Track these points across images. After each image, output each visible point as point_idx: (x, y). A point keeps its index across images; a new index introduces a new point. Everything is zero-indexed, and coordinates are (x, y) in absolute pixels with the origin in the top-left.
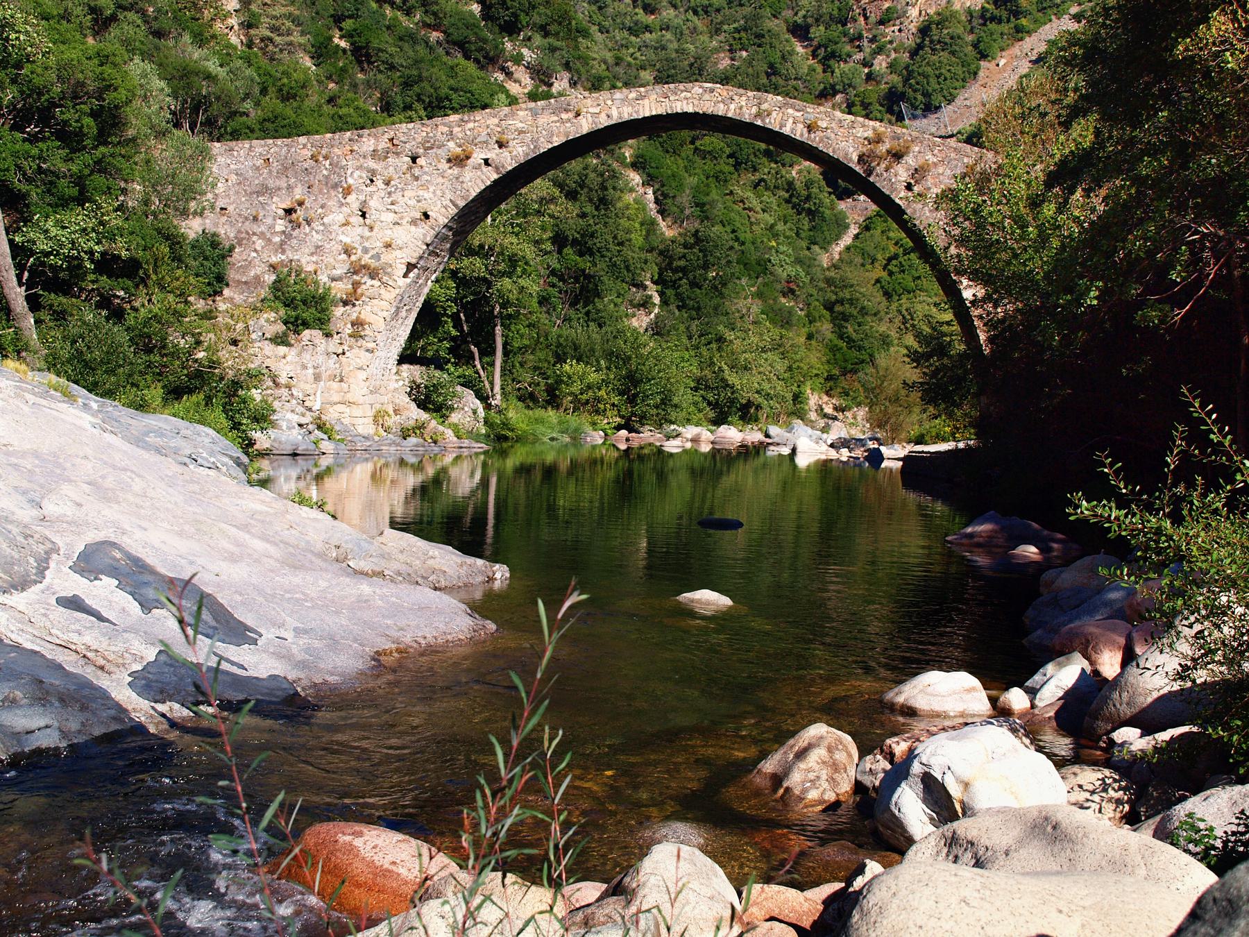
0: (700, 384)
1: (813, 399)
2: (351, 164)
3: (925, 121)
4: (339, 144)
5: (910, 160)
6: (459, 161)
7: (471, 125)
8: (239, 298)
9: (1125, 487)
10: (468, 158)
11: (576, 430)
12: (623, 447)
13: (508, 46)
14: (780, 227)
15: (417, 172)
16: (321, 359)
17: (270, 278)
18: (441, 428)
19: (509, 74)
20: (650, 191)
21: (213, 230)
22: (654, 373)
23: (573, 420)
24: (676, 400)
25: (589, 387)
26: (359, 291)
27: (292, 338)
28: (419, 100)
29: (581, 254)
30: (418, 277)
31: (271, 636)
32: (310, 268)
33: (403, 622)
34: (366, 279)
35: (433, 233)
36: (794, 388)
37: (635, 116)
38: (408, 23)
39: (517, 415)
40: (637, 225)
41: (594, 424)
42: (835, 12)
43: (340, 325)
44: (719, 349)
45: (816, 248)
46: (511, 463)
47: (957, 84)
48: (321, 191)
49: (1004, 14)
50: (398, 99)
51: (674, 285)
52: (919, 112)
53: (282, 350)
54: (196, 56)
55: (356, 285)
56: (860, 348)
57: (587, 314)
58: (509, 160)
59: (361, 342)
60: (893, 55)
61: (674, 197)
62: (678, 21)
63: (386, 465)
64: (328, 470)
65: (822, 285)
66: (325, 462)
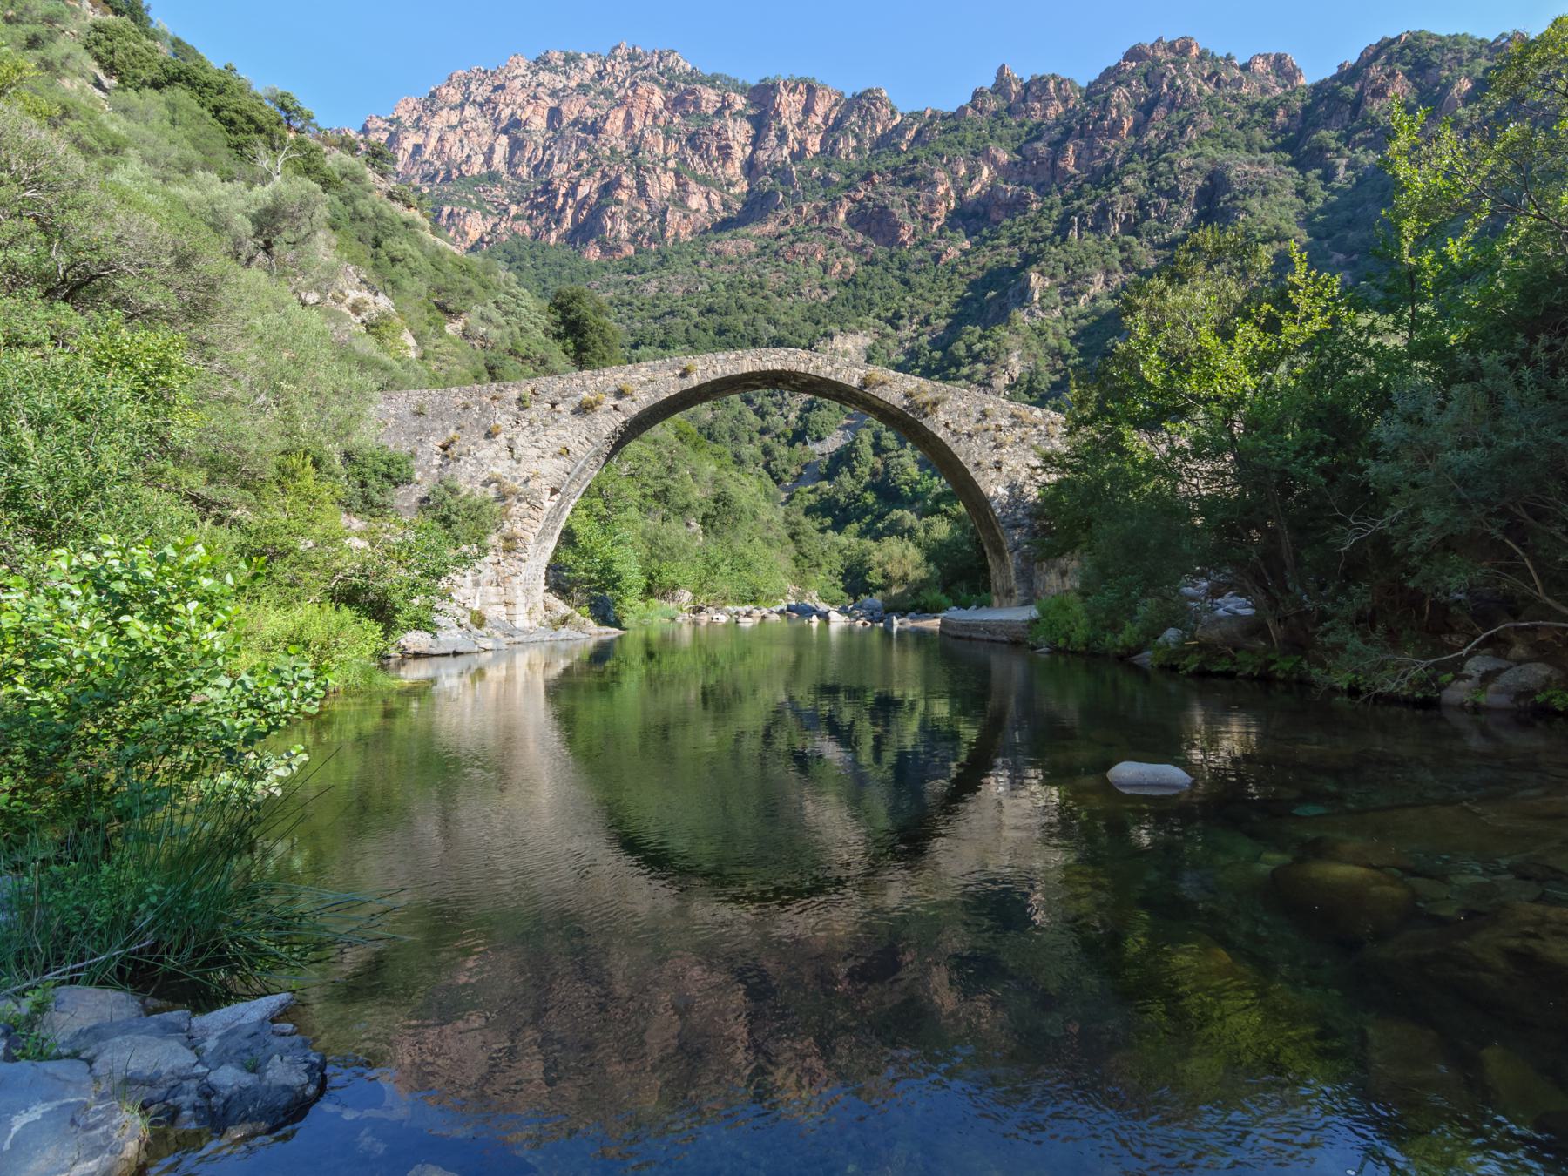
7: (601, 379)
37: (736, 373)
58: (633, 408)
59: (513, 554)
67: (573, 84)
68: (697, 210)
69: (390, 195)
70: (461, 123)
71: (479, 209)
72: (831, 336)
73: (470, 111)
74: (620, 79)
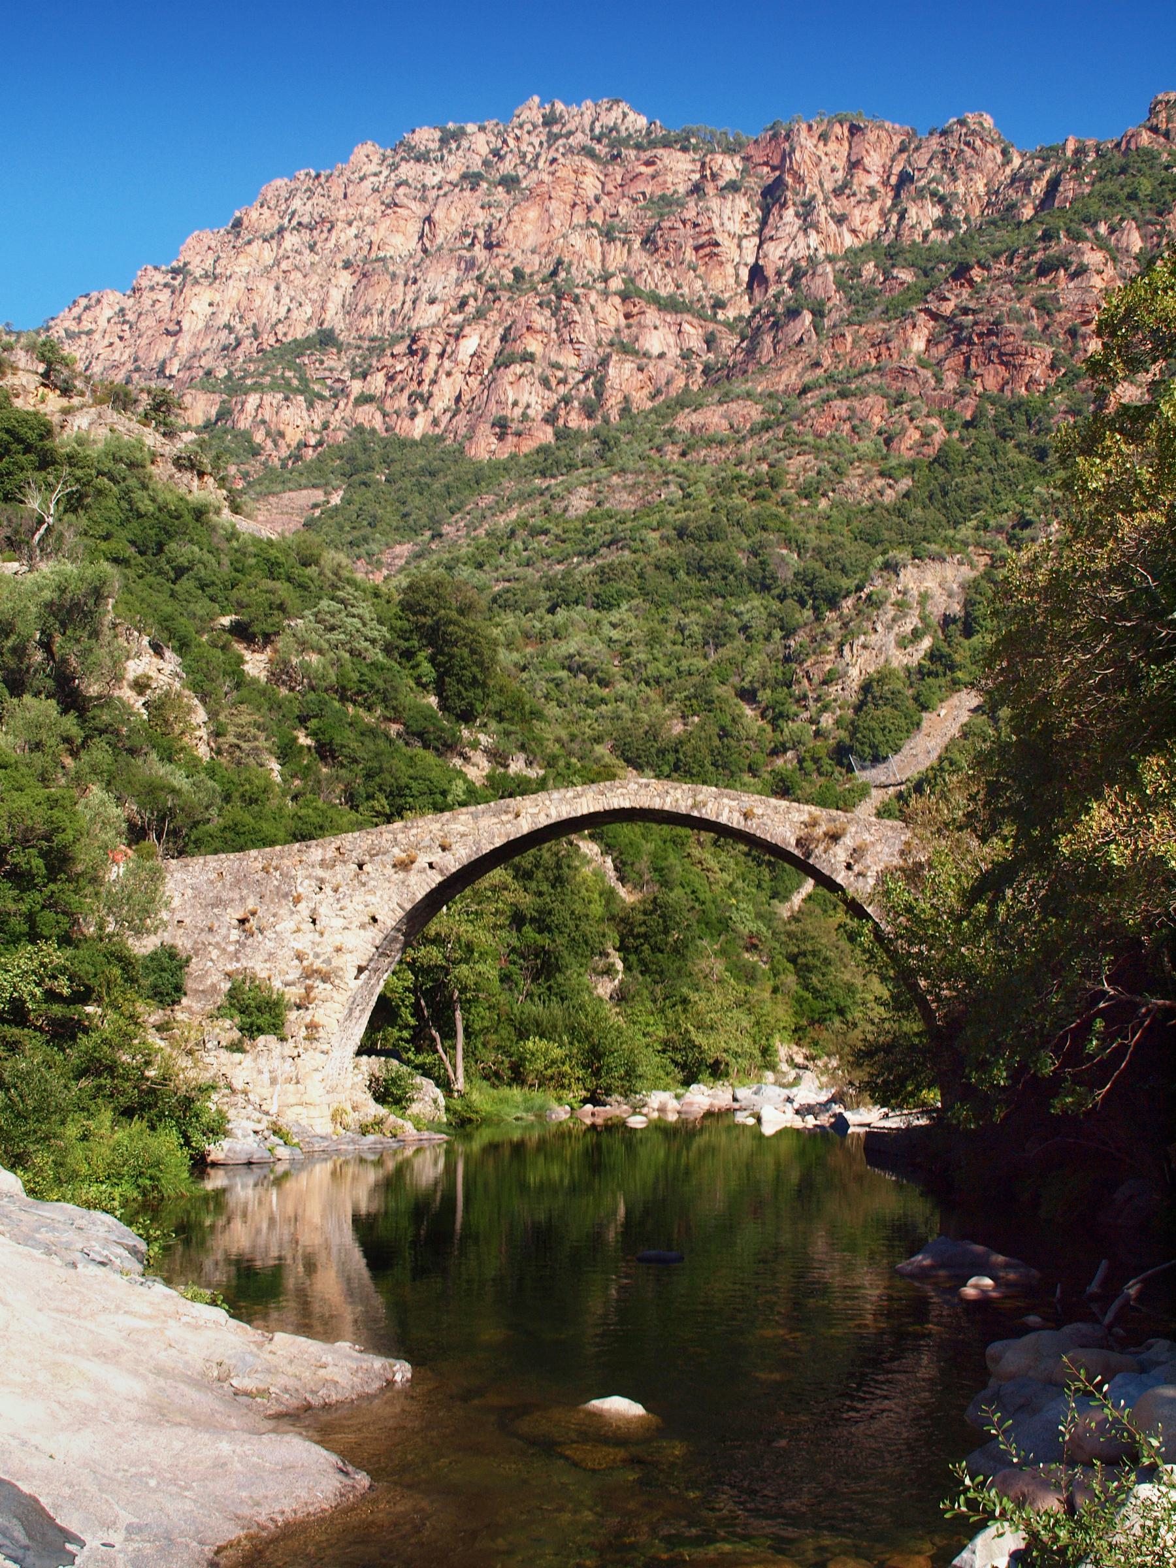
0: (667, 1046)
1: (783, 1049)
2: (300, 873)
3: (874, 771)
4: (288, 855)
5: (848, 841)
6: (404, 865)
7: (414, 831)
8: (196, 1006)
9: (1018, 1456)
10: (412, 862)
11: (541, 1108)
12: (588, 1121)
13: (465, 733)
14: (739, 884)
15: (364, 878)
16: (276, 1063)
17: (226, 986)
18: (400, 1121)
19: (467, 759)
20: (609, 860)
21: (171, 942)
22: (616, 1046)
23: (538, 1096)
24: (640, 1070)
25: (553, 1062)
26: (312, 995)
27: (247, 1044)
28: (380, 790)
29: (540, 932)
30: (370, 978)
31: (97, 1543)
32: (264, 975)
33: (258, 1493)
34: (318, 983)
35: (382, 936)
36: (763, 1042)
37: (573, 814)
38: (369, 719)
39: (482, 1098)
40: (596, 896)
41: (559, 1099)
42: (780, 676)
43: (294, 1029)
44: (685, 1011)
45: (775, 902)
46: (476, 1146)
47: (902, 735)
48: (272, 901)
49: (941, 669)
50: (362, 790)
51: (637, 950)
52: (868, 763)
53: (238, 1056)
54: (162, 772)
55: (309, 989)
56: (826, 998)
57: (549, 988)
58: (453, 862)
59: (315, 1044)
60: (838, 712)
61: (633, 864)
62: (633, 692)
63: (346, 1162)
64: (286, 1174)
65: (783, 938)
66: (280, 1168)
67: (454, 176)
68: (662, 356)
69: (178, 462)
70: (277, 262)
71: (302, 393)
72: (892, 568)
73: (291, 240)
74: (529, 157)
